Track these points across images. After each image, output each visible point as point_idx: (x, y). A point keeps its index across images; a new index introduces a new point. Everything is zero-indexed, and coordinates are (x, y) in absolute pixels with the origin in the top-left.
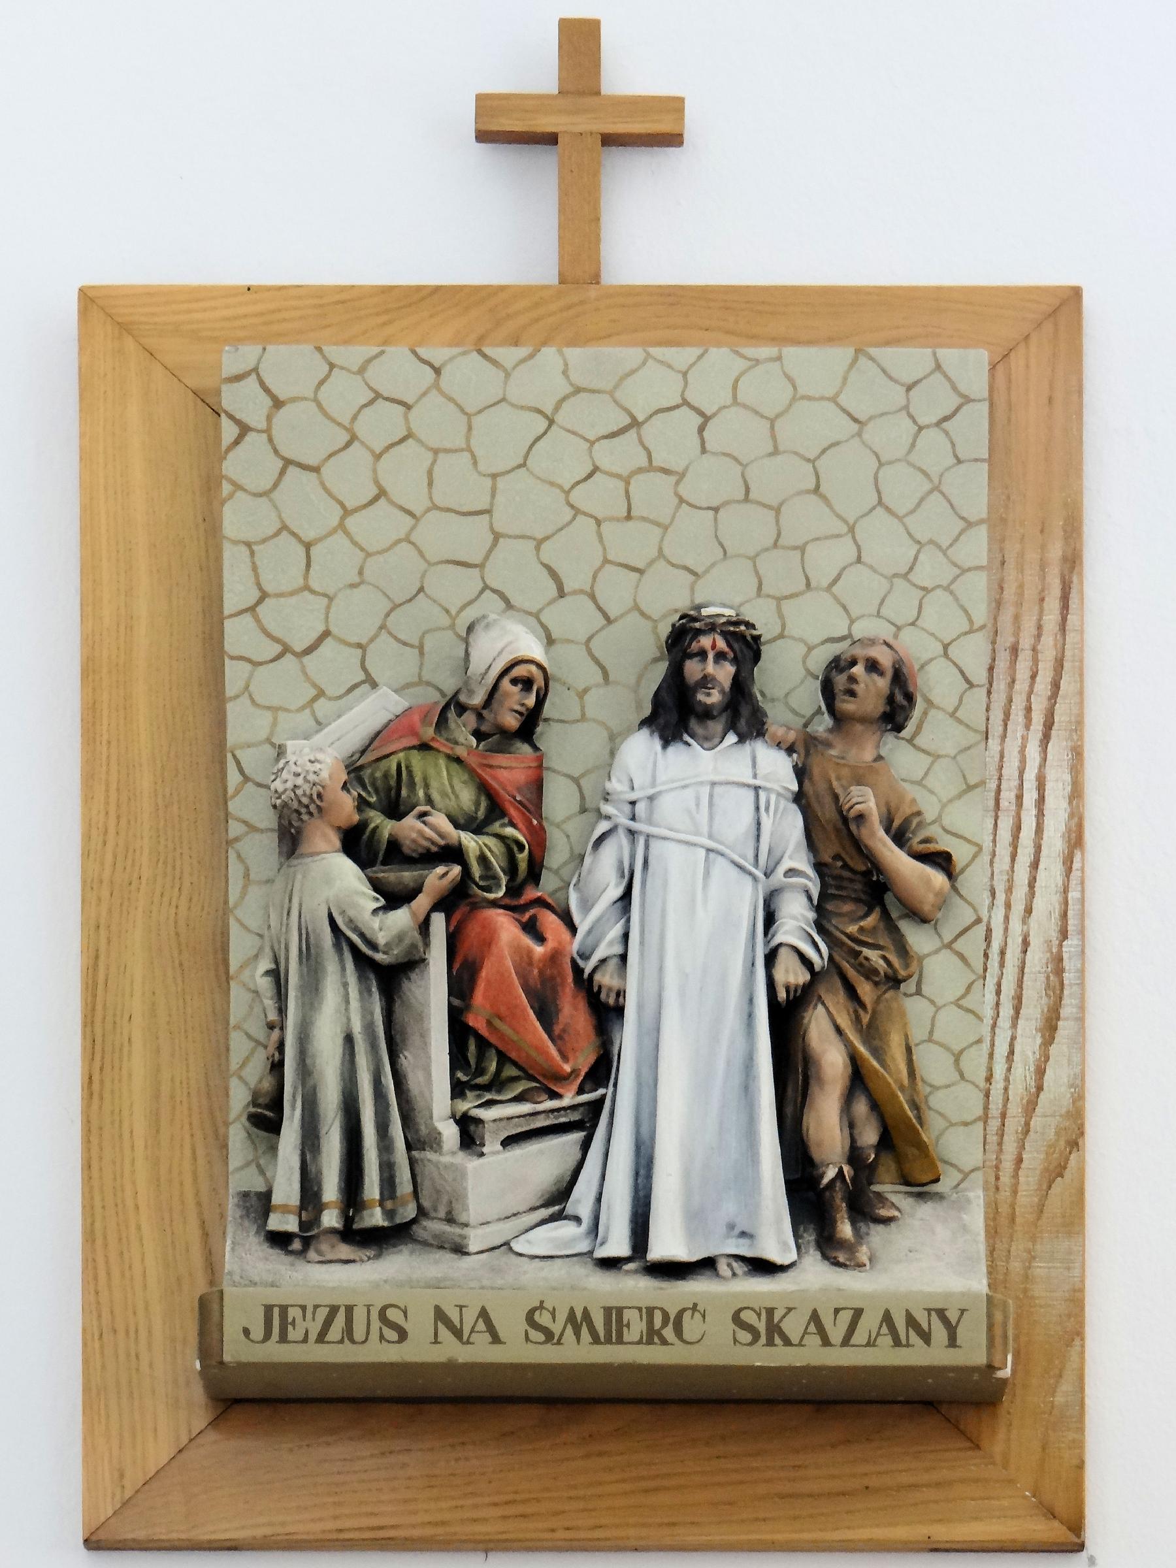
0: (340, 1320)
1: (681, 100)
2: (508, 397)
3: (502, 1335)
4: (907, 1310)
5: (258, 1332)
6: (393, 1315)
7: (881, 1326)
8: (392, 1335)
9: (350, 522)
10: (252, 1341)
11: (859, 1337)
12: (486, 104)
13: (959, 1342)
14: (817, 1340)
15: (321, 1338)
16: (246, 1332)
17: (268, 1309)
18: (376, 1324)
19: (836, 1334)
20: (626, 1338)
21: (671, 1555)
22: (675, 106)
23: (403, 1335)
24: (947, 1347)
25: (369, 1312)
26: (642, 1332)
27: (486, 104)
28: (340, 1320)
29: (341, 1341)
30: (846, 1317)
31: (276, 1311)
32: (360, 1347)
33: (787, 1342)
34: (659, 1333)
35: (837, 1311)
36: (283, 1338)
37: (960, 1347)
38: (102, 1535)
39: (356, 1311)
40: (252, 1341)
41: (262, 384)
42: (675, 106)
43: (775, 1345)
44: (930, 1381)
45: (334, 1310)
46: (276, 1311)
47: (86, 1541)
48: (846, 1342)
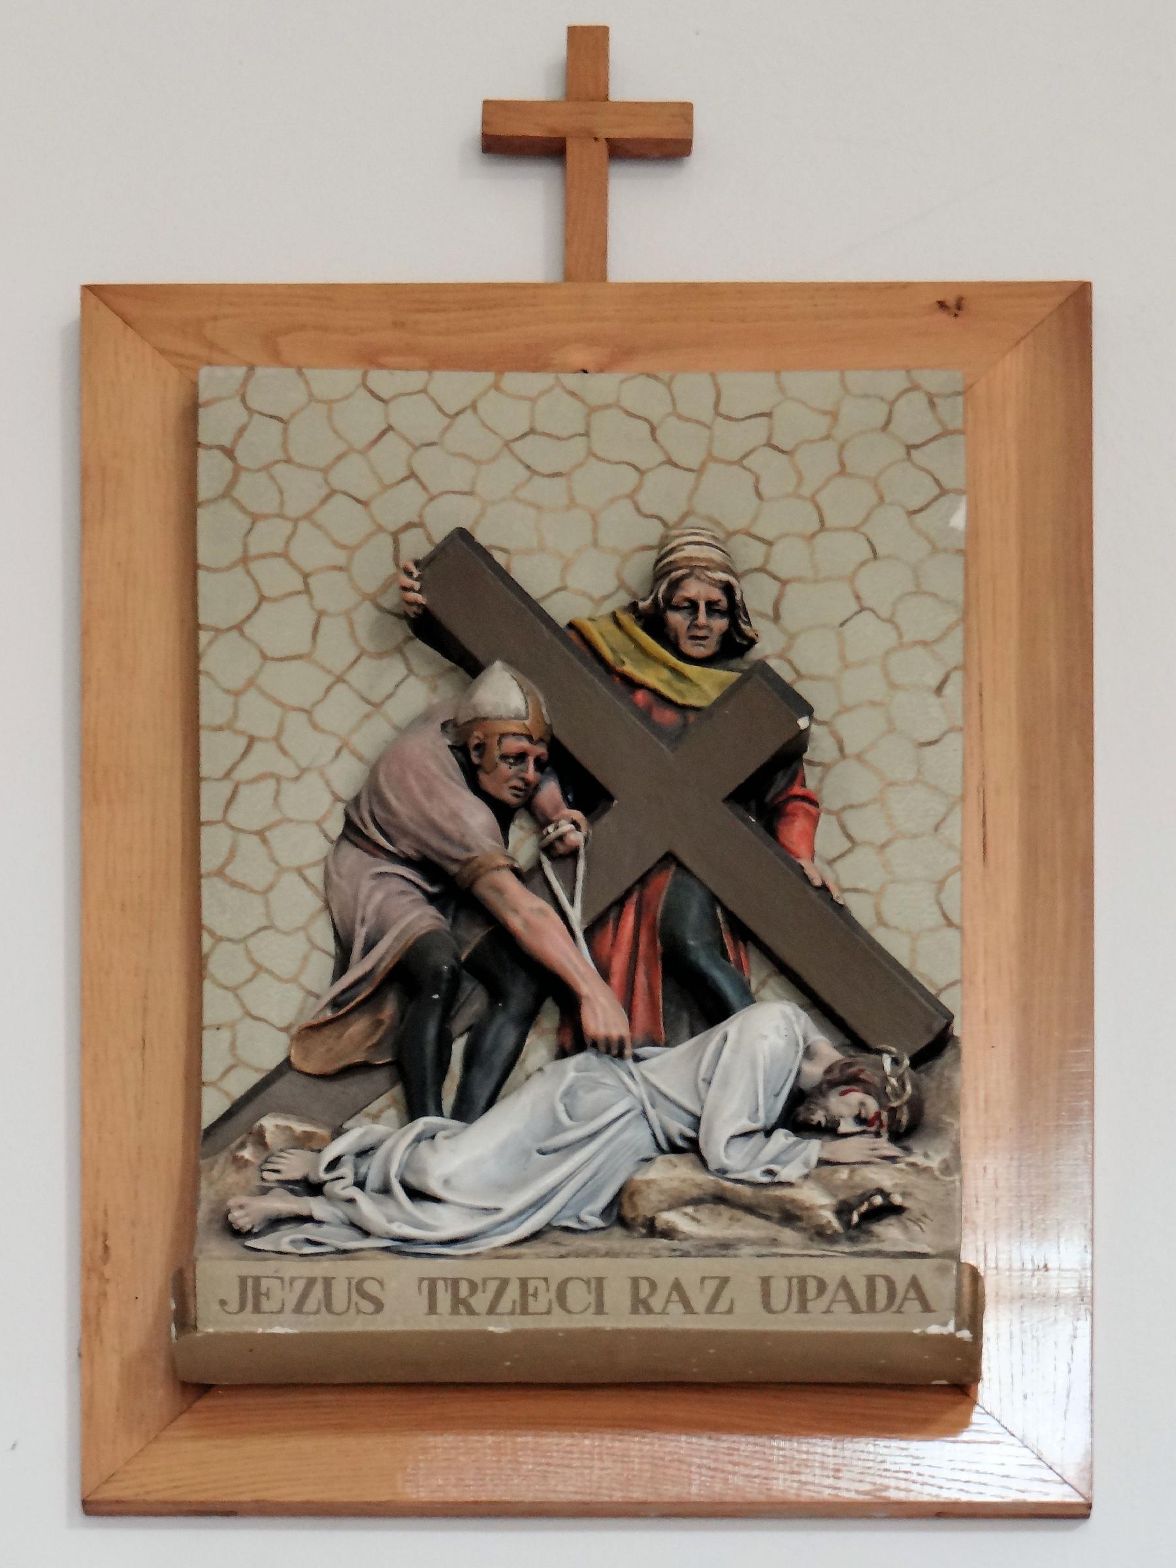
0: (318, 1292)
1: (605, 30)
2: (764, 441)
3: (933, 1305)
4: (677, 1279)
5: (234, 1305)
6: (371, 1288)
7: (670, 1295)
8: (367, 1306)
9: (304, 526)
10: (339, 1314)
11: (722, 1305)
12: (491, 108)
13: (606, 1309)
14: (847, 1307)
15: (299, 1308)
16: (223, 1303)
17: (243, 1280)
18: (355, 1297)
19: (699, 1301)
20: (531, 1308)
21: (443, 1522)
22: (684, 111)
23: (379, 1306)
24: (427, 1314)
25: (350, 1283)
26: (514, 1302)
27: (491, 108)
28: (318, 1292)
29: (317, 1312)
30: (711, 1287)
31: (250, 1283)
32: (780, 1317)
33: (649, 1311)
34: (465, 1303)
35: (703, 1279)
36: (257, 1309)
37: (934, 1311)
38: (111, 1492)
39: (334, 1283)
40: (339, 1314)
41: (517, 439)
42: (684, 111)
43: (461, 1314)
44: (712, 1351)
45: (311, 1282)
46: (250, 1283)
47: (84, 1503)
48: (710, 1309)
